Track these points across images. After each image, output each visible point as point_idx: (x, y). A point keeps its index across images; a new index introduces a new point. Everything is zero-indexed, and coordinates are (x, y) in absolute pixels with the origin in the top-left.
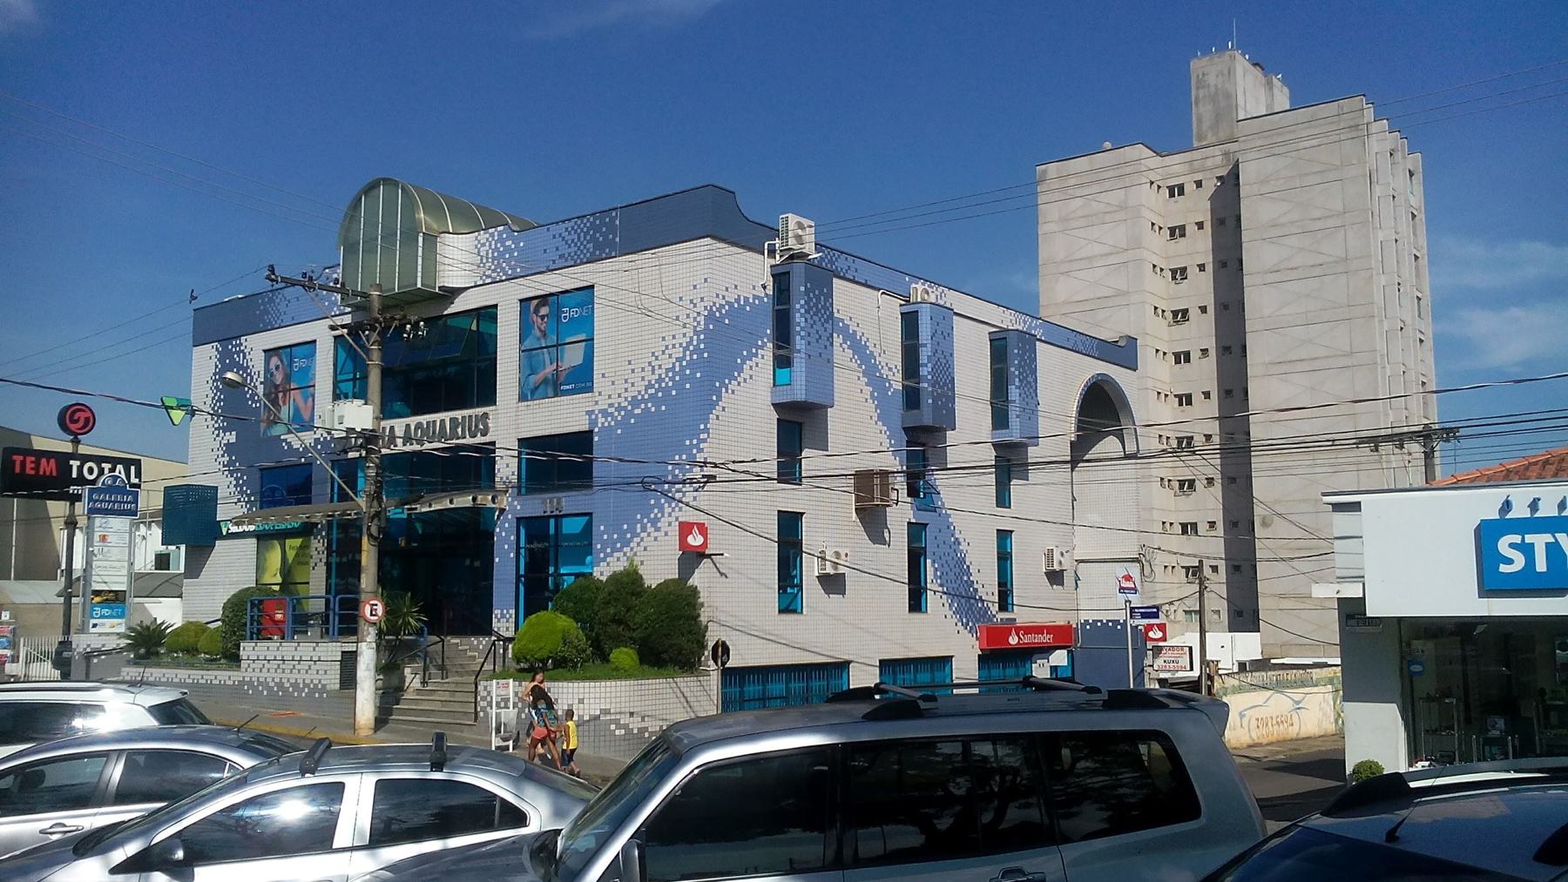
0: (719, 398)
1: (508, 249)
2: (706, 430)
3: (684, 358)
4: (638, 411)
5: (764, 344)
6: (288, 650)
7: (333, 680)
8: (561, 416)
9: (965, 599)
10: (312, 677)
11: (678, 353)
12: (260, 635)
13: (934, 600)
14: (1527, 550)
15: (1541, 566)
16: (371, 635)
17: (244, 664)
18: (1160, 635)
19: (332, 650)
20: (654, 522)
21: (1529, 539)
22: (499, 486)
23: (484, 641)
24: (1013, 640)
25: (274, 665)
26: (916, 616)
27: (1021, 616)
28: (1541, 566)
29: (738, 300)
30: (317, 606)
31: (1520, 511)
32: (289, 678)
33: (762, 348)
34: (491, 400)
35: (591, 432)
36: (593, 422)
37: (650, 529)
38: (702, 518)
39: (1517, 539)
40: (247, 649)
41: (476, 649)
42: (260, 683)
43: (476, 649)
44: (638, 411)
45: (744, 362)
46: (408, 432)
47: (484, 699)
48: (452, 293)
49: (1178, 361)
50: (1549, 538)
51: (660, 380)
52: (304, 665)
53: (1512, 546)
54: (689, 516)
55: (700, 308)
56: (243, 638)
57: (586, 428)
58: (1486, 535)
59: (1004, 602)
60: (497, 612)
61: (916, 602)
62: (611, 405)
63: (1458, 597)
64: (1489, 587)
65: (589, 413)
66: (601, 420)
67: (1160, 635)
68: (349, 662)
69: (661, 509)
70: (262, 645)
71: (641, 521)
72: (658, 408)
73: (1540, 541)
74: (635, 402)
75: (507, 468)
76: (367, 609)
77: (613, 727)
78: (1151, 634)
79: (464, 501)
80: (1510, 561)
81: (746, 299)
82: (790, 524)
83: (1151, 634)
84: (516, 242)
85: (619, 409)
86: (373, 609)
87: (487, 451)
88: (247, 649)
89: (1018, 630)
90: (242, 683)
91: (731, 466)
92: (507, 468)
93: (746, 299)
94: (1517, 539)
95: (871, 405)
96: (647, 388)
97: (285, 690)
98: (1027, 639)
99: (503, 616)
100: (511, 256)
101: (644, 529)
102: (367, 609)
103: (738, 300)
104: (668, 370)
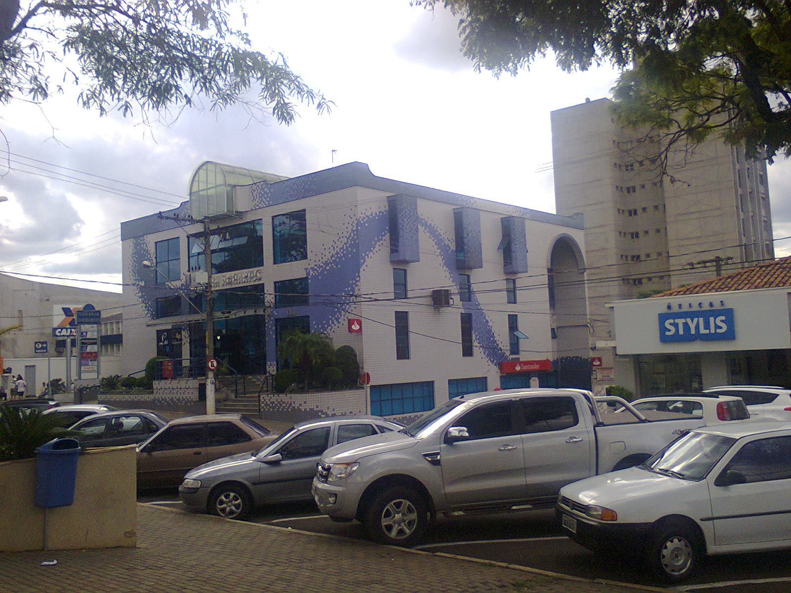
0: (365, 261)
1: (265, 193)
2: (359, 276)
3: (348, 242)
4: (328, 268)
5: (385, 234)
6: (174, 383)
7: (195, 396)
8: (293, 270)
9: (493, 351)
10: (186, 396)
11: (345, 240)
12: (163, 378)
13: (477, 350)
14: (676, 325)
15: (681, 332)
16: (211, 375)
17: (155, 391)
18: (598, 363)
19: (194, 383)
20: (337, 320)
21: (677, 321)
22: (267, 304)
23: (263, 377)
24: (518, 368)
25: (168, 391)
26: (468, 359)
27: (523, 357)
28: (681, 332)
29: (372, 215)
30: (186, 363)
31: (675, 309)
32: (176, 396)
33: (384, 236)
34: (261, 264)
35: (307, 278)
36: (308, 274)
37: (335, 322)
38: (357, 318)
39: (672, 321)
40: (156, 384)
41: (258, 380)
42: (162, 399)
43: (258, 380)
44: (328, 268)
45: (375, 244)
46: (222, 281)
47: (263, 403)
48: (240, 214)
49: (630, 215)
50: (683, 320)
51: (337, 253)
52: (182, 391)
53: (670, 324)
54: (351, 317)
55: (354, 219)
56: (154, 379)
57: (305, 276)
58: (663, 318)
59: (515, 347)
60: (268, 363)
61: (468, 351)
62: (316, 265)
63: (652, 345)
64: (664, 339)
65: (306, 269)
66: (311, 272)
67: (598, 363)
68: (202, 389)
69: (340, 314)
70: (163, 382)
71: (331, 319)
72: (337, 266)
73: (680, 322)
74: (326, 264)
75: (270, 297)
76: (210, 364)
77: (320, 414)
78: (594, 363)
79: (250, 312)
80: (670, 330)
81: (376, 213)
82: (402, 319)
83: (594, 363)
84: (269, 189)
85: (320, 267)
86: (213, 364)
87: (260, 288)
88: (156, 384)
89: (520, 363)
90: (155, 400)
91: (364, 296)
92: (270, 297)
93: (376, 213)
94: (672, 321)
95: (440, 258)
96: (331, 257)
97: (174, 402)
98: (526, 368)
99: (271, 365)
100: (268, 197)
101: (333, 323)
102: (210, 364)
103: (372, 215)
104: (340, 249)
